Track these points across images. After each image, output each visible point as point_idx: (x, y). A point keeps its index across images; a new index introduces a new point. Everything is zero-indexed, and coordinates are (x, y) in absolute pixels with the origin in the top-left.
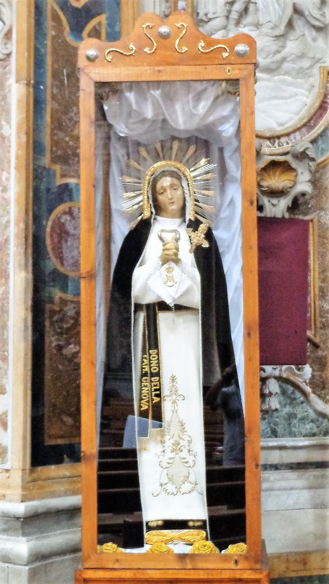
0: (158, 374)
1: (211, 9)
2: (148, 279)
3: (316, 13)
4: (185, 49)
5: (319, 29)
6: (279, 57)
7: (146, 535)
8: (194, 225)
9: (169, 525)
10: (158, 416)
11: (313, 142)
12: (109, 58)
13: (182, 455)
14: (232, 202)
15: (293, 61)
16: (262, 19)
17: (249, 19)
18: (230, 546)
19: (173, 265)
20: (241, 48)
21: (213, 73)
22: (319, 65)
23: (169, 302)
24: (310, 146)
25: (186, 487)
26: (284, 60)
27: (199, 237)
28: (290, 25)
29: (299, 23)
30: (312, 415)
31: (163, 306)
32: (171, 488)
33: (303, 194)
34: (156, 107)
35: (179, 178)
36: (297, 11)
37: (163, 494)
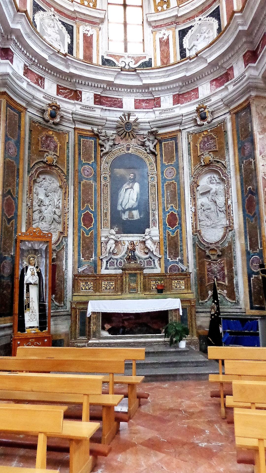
0: (29, 297)
1: (36, 218)
2: (28, 278)
3: (58, 220)
4: (39, 235)
5: (58, 223)
6: (50, 228)
7: (26, 330)
8: (37, 267)
9: (30, 327)
10: (29, 307)
11: (56, 247)
12: (23, 235)
13: (33, 313)
14: (43, 262)
15: (53, 230)
16: (46, 220)
17: (44, 220)
18: (218, 26)
19: (34, 276)
20: (49, 235)
21: (44, 240)
22: (58, 230)
23: (32, 283)
24: (56, 248)
25: (34, 320)
26: (51, 229)
27: (38, 270)
28: (52, 222)
29: (54, 221)
30: (54, 305)
31: (31, 284)
32: (31, 320)
33: (54, 258)
34: (32, 244)
35: (34, 258)
36: (54, 219)
37: (30, 322)
